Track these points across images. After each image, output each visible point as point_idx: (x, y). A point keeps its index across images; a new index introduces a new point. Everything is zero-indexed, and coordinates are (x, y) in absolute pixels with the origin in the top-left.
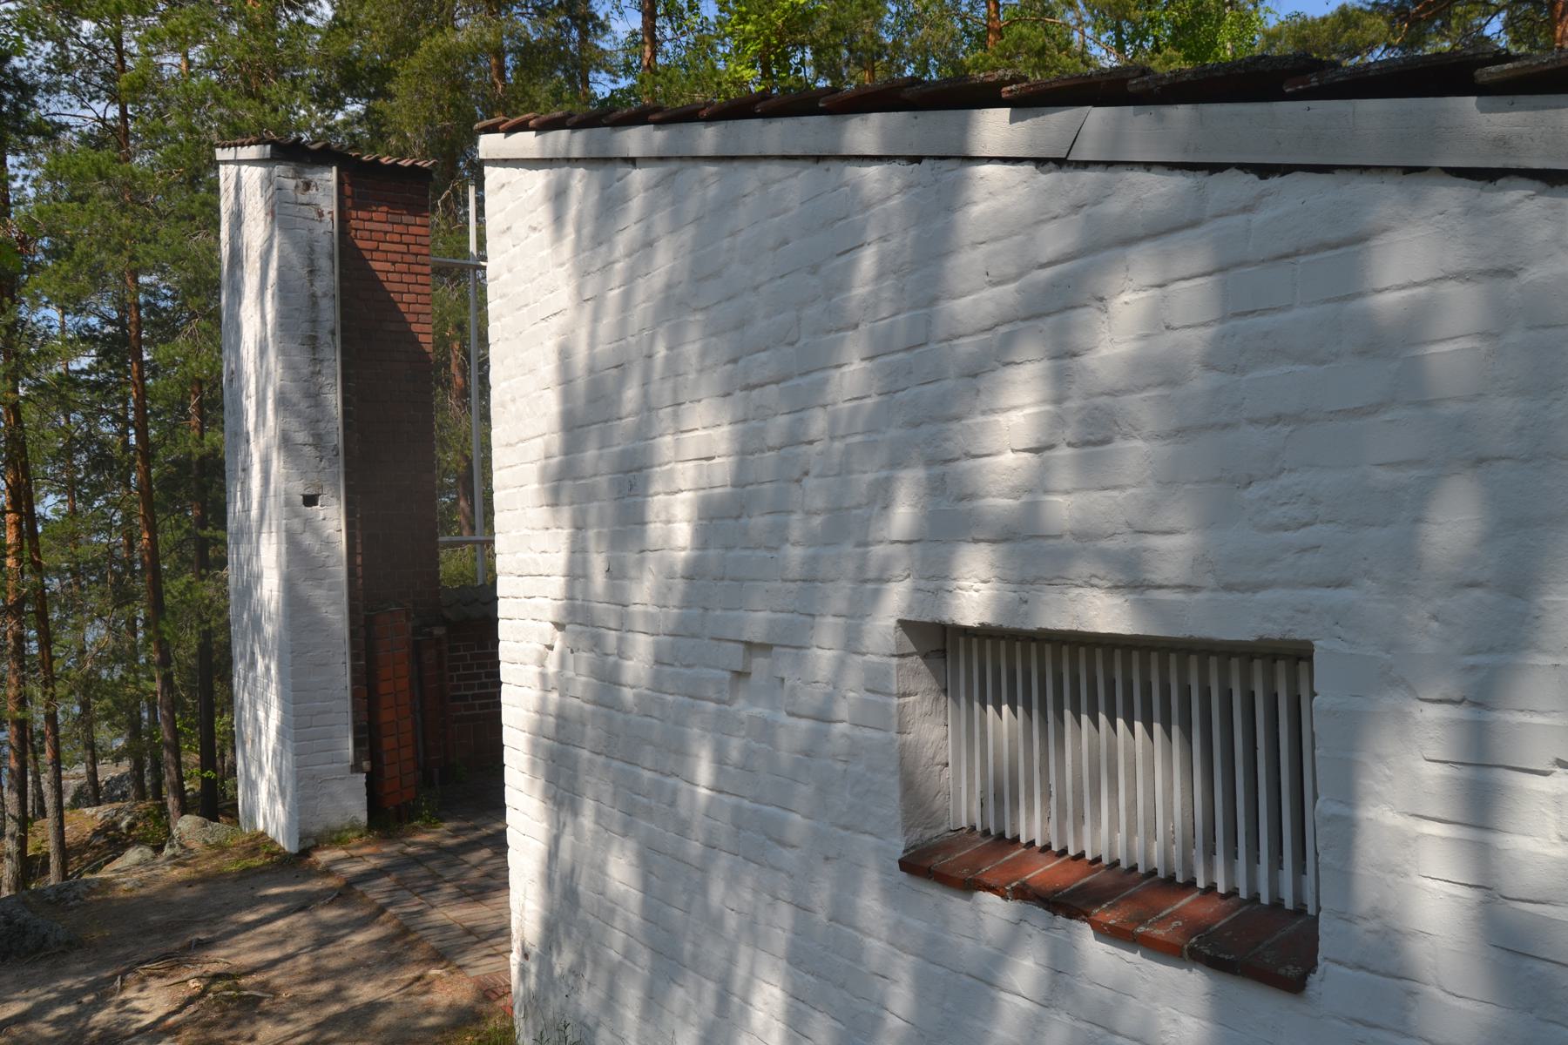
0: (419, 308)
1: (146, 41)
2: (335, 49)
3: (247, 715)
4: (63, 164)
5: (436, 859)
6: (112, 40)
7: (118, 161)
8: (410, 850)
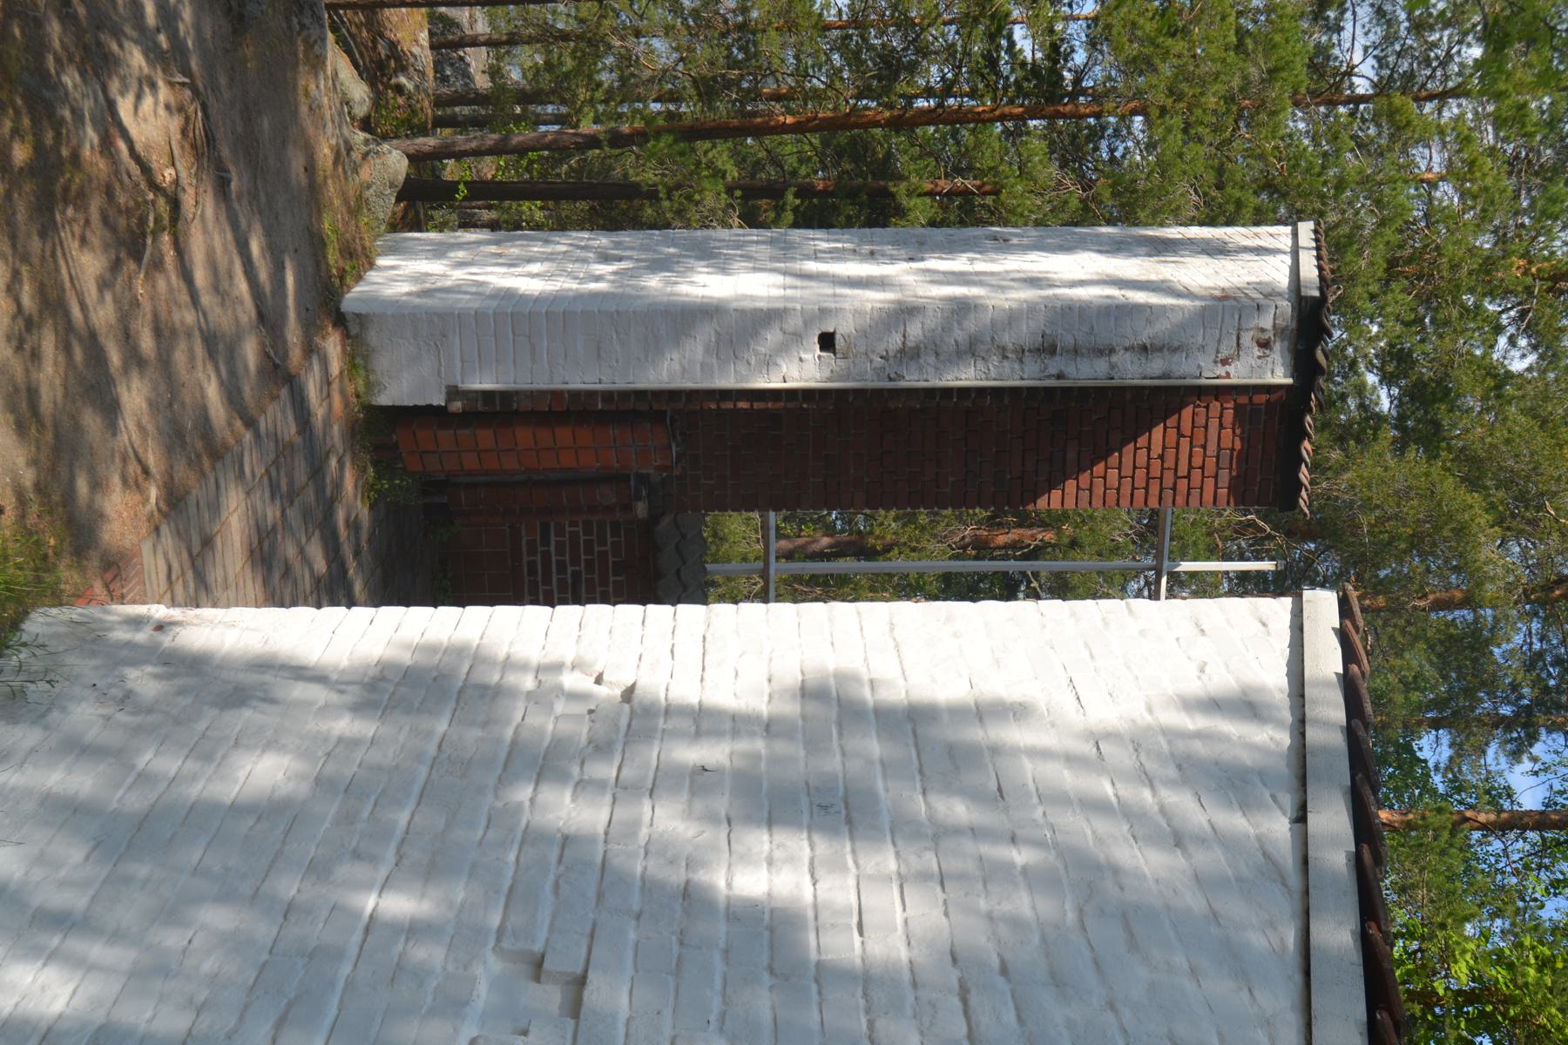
0: (1099, 490)
1: (1459, 130)
2: (1463, 377)
3: (537, 248)
4: (1287, 25)
5: (317, 499)
6: (1459, 85)
7: (1296, 92)
8: (333, 462)
